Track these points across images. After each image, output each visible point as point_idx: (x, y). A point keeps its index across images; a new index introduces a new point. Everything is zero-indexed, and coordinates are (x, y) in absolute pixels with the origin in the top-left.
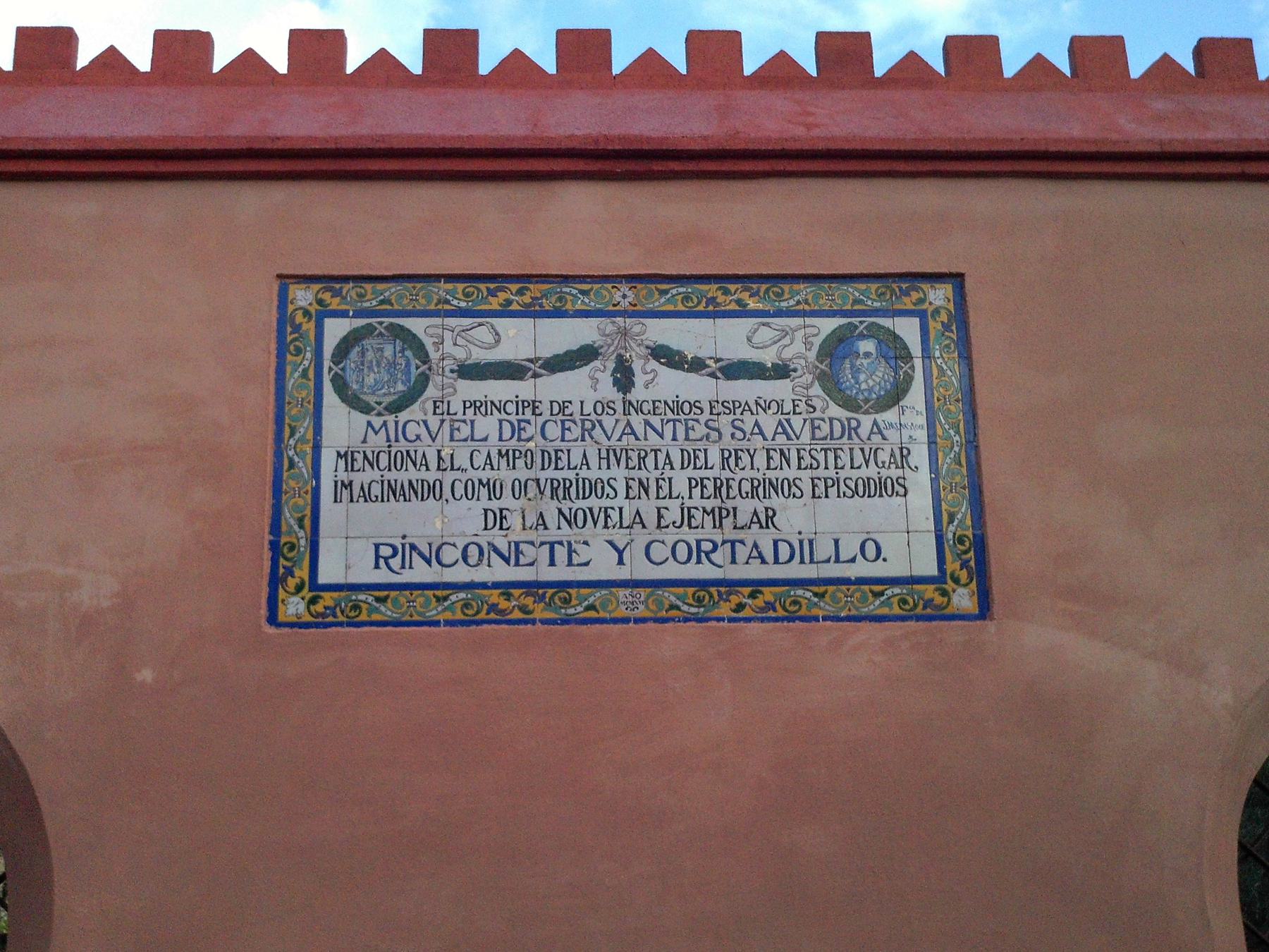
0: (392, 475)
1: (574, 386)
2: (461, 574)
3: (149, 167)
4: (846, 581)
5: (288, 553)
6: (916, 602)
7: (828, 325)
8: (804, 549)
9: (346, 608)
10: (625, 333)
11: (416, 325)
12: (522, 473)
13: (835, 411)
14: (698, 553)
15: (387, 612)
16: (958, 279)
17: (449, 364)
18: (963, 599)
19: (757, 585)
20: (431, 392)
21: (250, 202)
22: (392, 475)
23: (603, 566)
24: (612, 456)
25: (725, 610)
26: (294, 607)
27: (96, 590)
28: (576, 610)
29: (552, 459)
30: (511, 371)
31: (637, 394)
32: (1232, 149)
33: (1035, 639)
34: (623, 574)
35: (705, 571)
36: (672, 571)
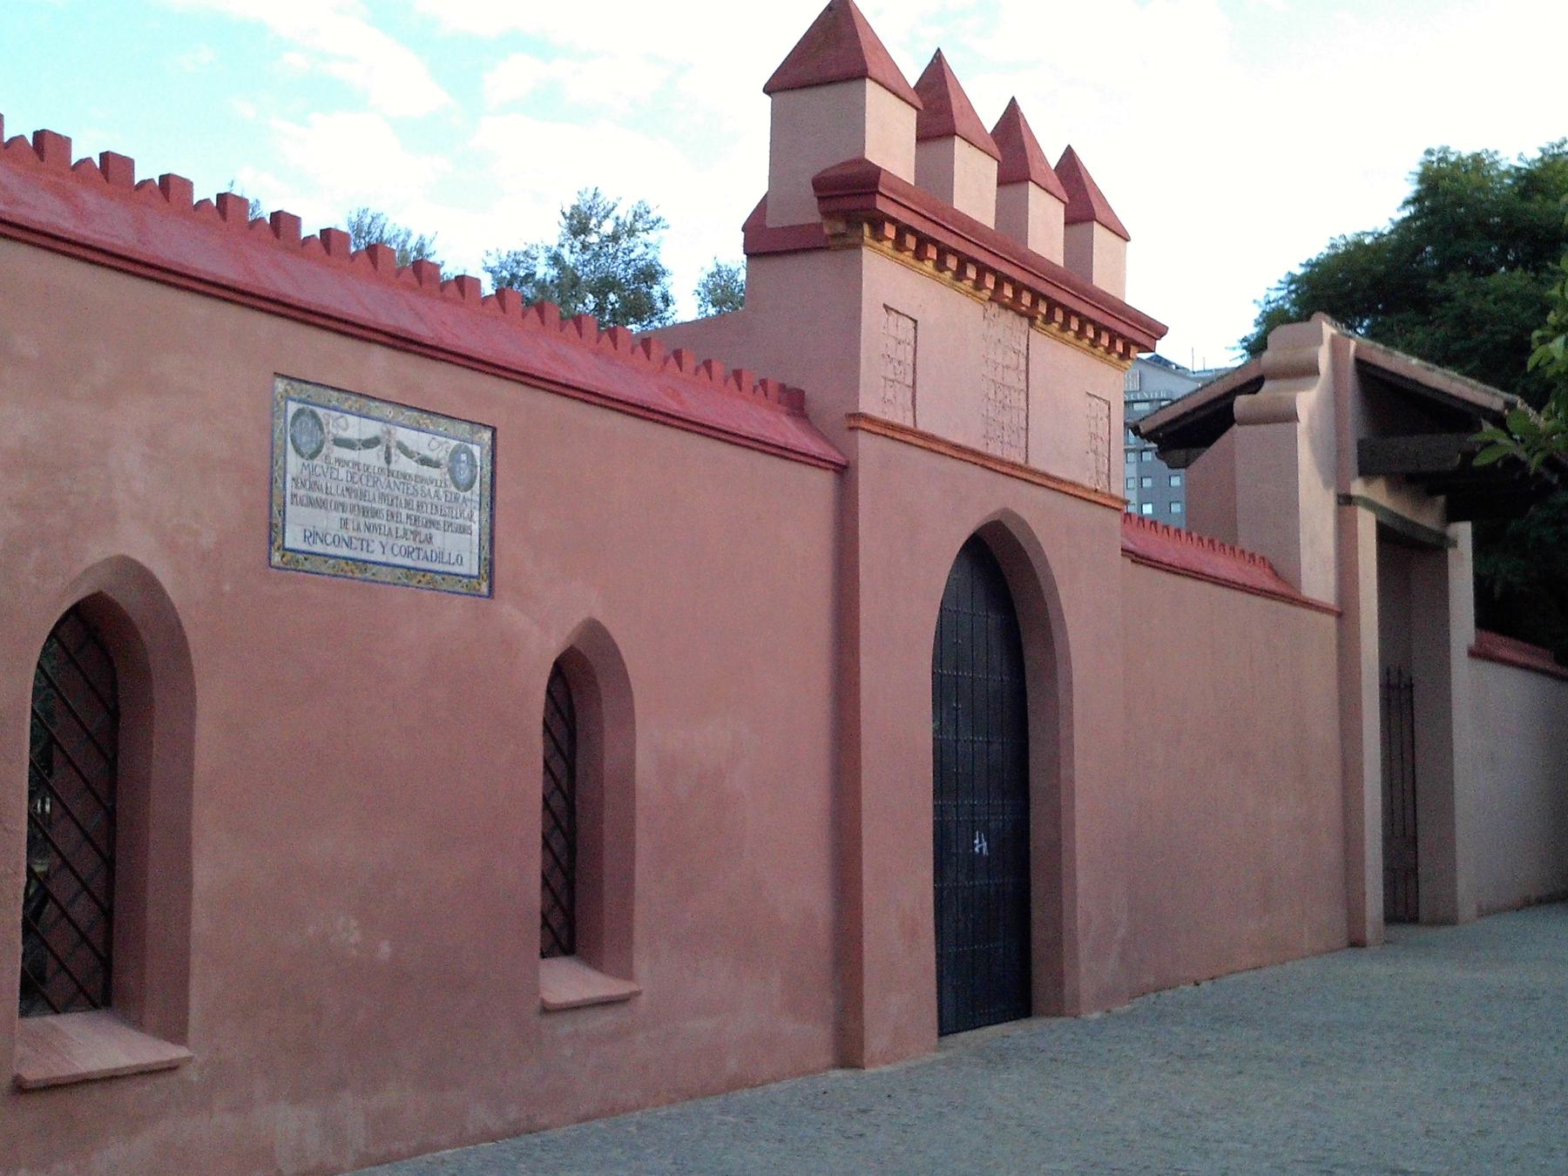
0: (311, 494)
1: (372, 457)
2: (331, 550)
3: (130, 267)
4: (449, 574)
5: (274, 531)
6: (462, 586)
7: (454, 443)
8: (439, 557)
9: (297, 562)
10: (389, 432)
11: (320, 412)
12: (354, 501)
13: (453, 489)
14: (408, 554)
15: (307, 566)
16: (494, 430)
17: (331, 437)
18: (484, 589)
19: (425, 571)
20: (324, 450)
21: (265, 326)
22: (311, 494)
23: (377, 556)
24: (383, 497)
25: (414, 582)
26: (276, 558)
27: (208, 540)
28: (368, 575)
29: (363, 495)
30: (348, 444)
31: (393, 467)
32: (208, 278)
33: (506, 610)
34: (383, 559)
35: (408, 562)
36: (399, 561)
